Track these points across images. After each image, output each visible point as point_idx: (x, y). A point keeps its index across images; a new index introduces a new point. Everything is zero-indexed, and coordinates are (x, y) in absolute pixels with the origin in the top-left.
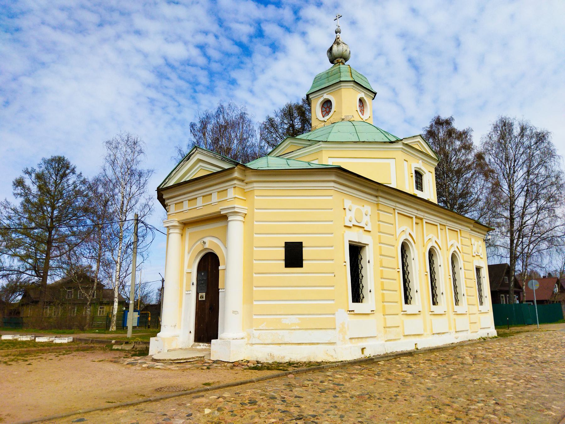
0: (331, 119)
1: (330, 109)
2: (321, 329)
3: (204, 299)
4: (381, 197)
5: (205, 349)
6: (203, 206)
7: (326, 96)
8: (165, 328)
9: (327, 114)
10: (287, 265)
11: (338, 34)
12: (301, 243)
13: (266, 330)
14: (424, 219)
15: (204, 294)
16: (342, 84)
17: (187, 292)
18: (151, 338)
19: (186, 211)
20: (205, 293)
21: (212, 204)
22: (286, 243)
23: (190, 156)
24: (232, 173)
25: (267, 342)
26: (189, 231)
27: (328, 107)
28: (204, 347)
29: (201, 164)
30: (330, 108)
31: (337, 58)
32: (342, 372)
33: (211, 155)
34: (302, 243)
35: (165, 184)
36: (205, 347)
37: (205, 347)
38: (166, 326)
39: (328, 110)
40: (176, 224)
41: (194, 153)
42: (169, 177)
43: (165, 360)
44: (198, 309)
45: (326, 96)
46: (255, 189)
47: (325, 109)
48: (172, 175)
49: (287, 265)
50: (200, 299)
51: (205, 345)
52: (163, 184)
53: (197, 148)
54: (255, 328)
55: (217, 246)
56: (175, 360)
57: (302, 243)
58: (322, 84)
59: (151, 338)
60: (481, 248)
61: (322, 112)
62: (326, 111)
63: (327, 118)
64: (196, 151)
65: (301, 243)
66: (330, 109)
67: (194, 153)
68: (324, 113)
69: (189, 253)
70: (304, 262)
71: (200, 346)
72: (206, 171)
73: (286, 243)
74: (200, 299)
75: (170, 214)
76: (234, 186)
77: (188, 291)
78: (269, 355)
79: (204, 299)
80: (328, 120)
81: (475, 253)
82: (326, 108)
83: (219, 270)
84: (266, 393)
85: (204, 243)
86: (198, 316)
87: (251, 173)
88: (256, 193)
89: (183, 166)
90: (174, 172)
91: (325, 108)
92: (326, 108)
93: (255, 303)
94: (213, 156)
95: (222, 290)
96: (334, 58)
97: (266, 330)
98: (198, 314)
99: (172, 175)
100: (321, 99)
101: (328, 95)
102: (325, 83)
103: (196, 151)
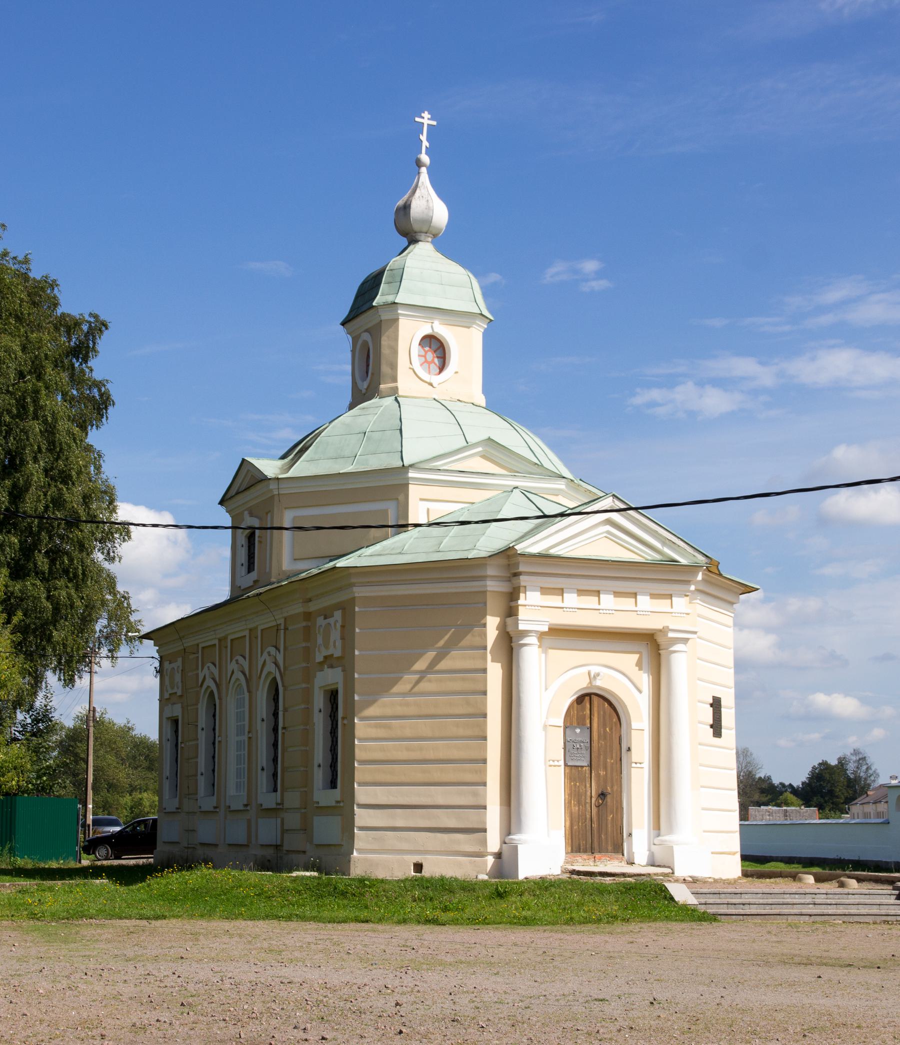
1: (426, 361)
100: (426, 330)
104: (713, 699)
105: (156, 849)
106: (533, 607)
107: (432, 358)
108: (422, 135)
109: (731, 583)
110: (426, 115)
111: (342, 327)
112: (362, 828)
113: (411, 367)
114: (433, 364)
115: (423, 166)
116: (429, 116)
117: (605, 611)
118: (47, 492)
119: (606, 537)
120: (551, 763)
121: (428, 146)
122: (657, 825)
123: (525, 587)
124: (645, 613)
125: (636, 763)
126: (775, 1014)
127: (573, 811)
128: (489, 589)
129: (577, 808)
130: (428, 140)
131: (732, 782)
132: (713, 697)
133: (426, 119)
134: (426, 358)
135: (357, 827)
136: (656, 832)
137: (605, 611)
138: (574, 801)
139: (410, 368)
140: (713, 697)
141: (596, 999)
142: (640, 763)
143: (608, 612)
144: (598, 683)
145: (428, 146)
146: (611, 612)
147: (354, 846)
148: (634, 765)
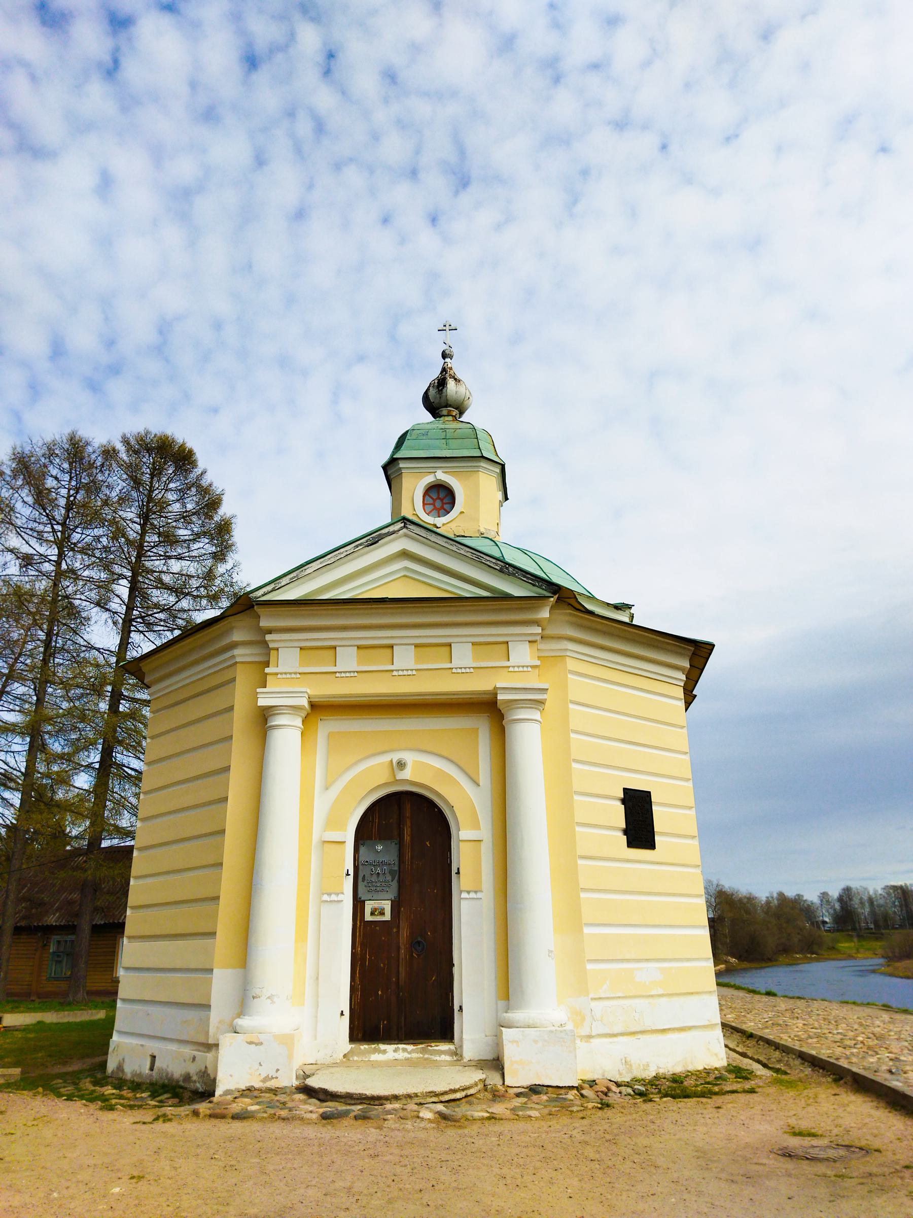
0: (452, 525)
2: (692, 993)
3: (387, 917)
5: (407, 1059)
6: (416, 670)
7: (442, 476)
8: (273, 1002)
11: (448, 360)
13: (608, 998)
15: (387, 906)
16: (483, 464)
20: (389, 902)
23: (381, 537)
24: (536, 609)
25: (616, 1030)
26: (326, 727)
27: (438, 498)
28: (401, 1055)
31: (450, 406)
33: (462, 552)
35: (273, 590)
36: (406, 1055)
37: (406, 1055)
38: (275, 999)
40: (304, 702)
41: (394, 533)
42: (297, 572)
43: (416, 1095)
44: (362, 944)
46: (568, 654)
47: (431, 501)
48: (308, 571)
50: (368, 917)
51: (404, 1050)
52: (269, 588)
53: (405, 524)
54: (592, 995)
56: (445, 1093)
58: (428, 448)
62: (433, 504)
64: (401, 529)
67: (394, 533)
71: (385, 1052)
72: (423, 587)
74: (368, 917)
75: (277, 674)
76: (531, 638)
78: (624, 1061)
79: (387, 917)
80: (444, 525)
82: (434, 500)
84: (651, 1157)
86: (363, 965)
87: (567, 618)
88: (571, 664)
89: (349, 557)
90: (316, 565)
91: (432, 498)
93: (587, 930)
94: (469, 555)
96: (444, 404)
97: (608, 998)
98: (363, 959)
99: (308, 571)
100: (429, 479)
102: (440, 449)
103: (401, 529)
106: (288, 676)
107: (441, 505)
109: (637, 631)
112: (123, 1000)
113: (414, 513)
114: (443, 510)
117: (401, 673)
119: (405, 576)
120: (326, 897)
122: (794, 971)
123: (277, 649)
124: (464, 672)
125: (468, 892)
128: (238, 659)
131: (702, 916)
134: (435, 506)
135: (120, 999)
136: (502, 1003)
137: (401, 673)
139: (414, 514)
141: (835, 1161)
142: (476, 892)
143: (405, 673)
144: (407, 774)
146: (410, 673)
147: (113, 1025)
148: (464, 895)
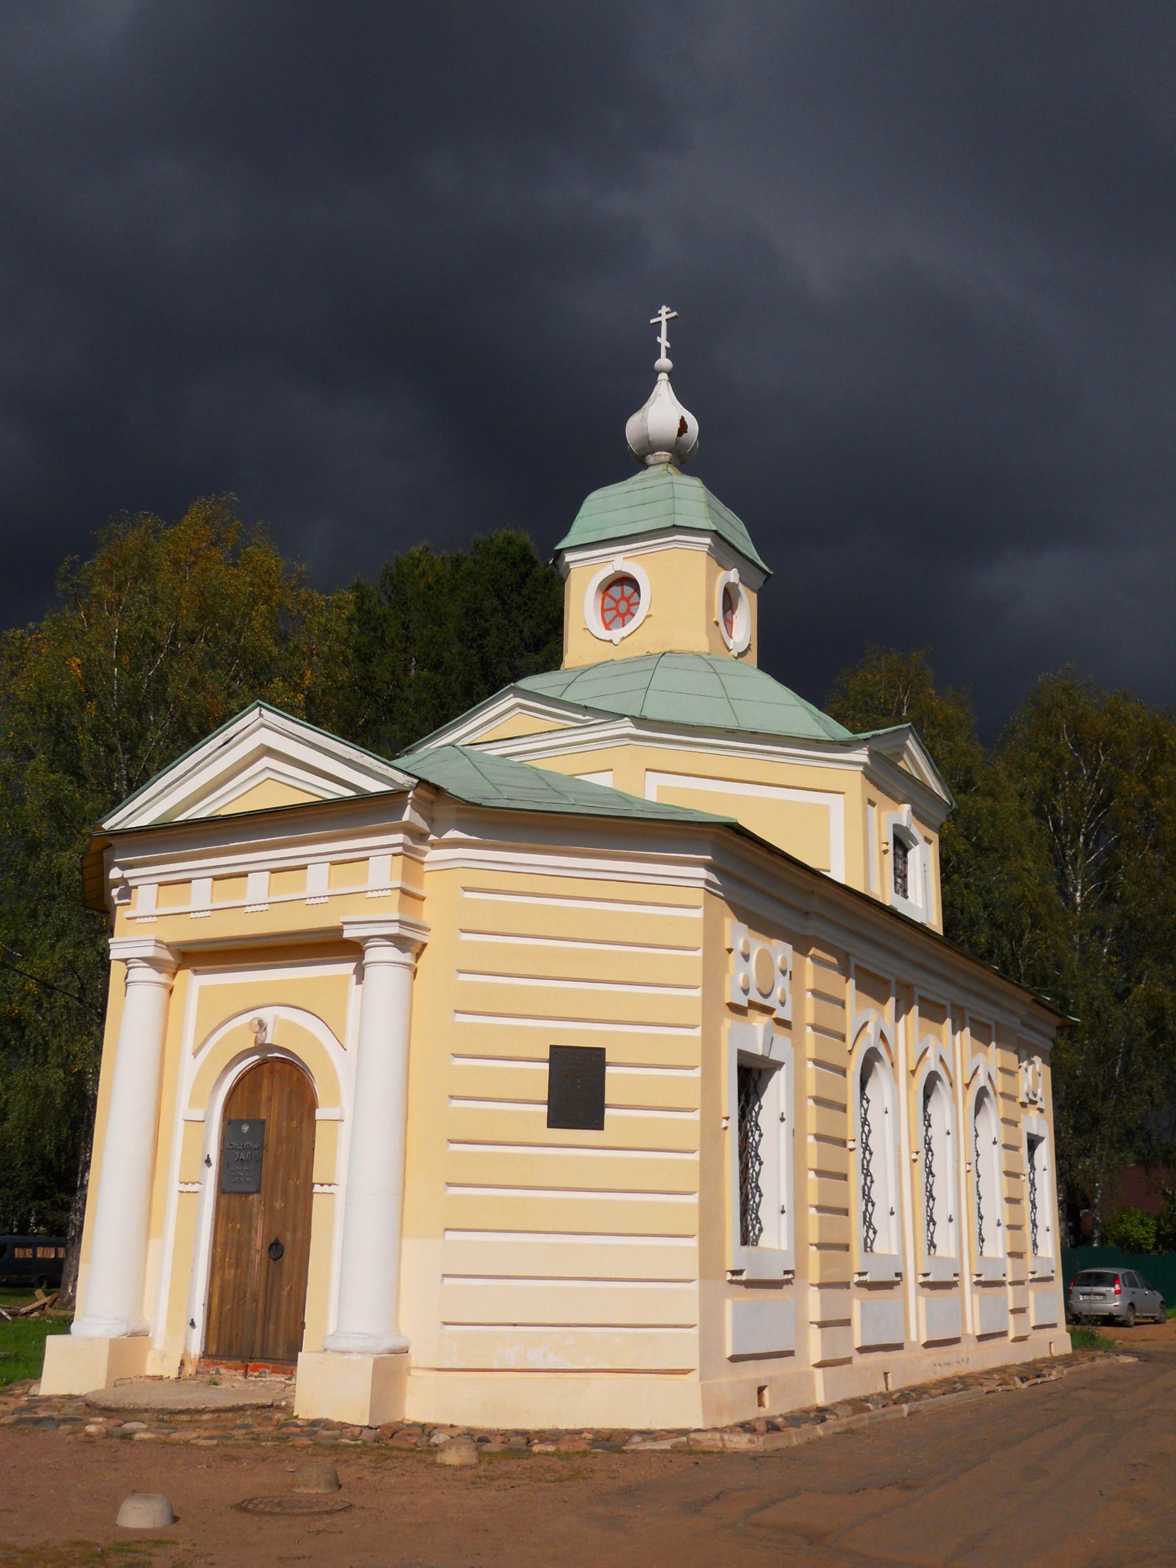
1: (630, 605)
4: (822, 917)
9: (619, 620)
10: (555, 1121)
12: (600, 1053)
14: (916, 989)
17: (195, 1188)
18: (48, 1337)
19: (202, 914)
21: (308, 901)
22: (552, 1047)
27: (623, 598)
29: (266, 761)
30: (632, 601)
32: (11, 1389)
34: (603, 1050)
39: (623, 607)
45: (620, 561)
47: (613, 604)
49: (555, 1121)
55: (312, 1040)
57: (603, 1050)
59: (48, 1337)
60: (1040, 1079)
61: (603, 610)
63: (617, 634)
65: (600, 1053)
66: (630, 605)
68: (610, 615)
69: (195, 1054)
70: (608, 1112)
73: (552, 1047)
77: (187, 1184)
81: (1027, 1095)
82: (617, 602)
83: (315, 1121)
85: (261, 1025)
91: (613, 599)
92: (617, 602)
95: (326, 1189)
101: (627, 562)
104: (977, 1053)
105: (64, 1326)
108: (660, 337)
110: (664, 309)
111: (746, 1246)
115: (645, 457)
116: (668, 309)
118: (82, 727)
121: (658, 338)
126: (409, 1438)
127: (226, 1276)
129: (233, 1272)
130: (659, 344)
132: (738, 1050)
133: (665, 314)
134: (628, 603)
138: (230, 1258)
140: (738, 1050)
145: (658, 338)
